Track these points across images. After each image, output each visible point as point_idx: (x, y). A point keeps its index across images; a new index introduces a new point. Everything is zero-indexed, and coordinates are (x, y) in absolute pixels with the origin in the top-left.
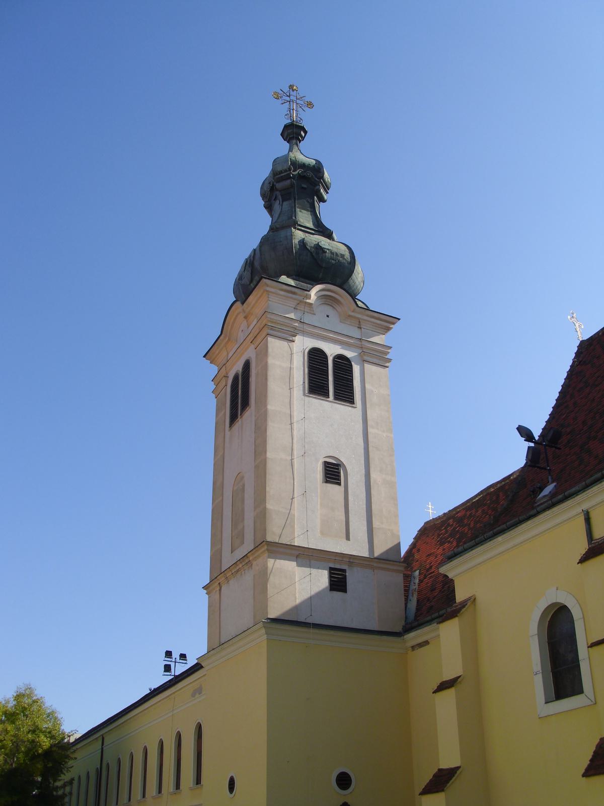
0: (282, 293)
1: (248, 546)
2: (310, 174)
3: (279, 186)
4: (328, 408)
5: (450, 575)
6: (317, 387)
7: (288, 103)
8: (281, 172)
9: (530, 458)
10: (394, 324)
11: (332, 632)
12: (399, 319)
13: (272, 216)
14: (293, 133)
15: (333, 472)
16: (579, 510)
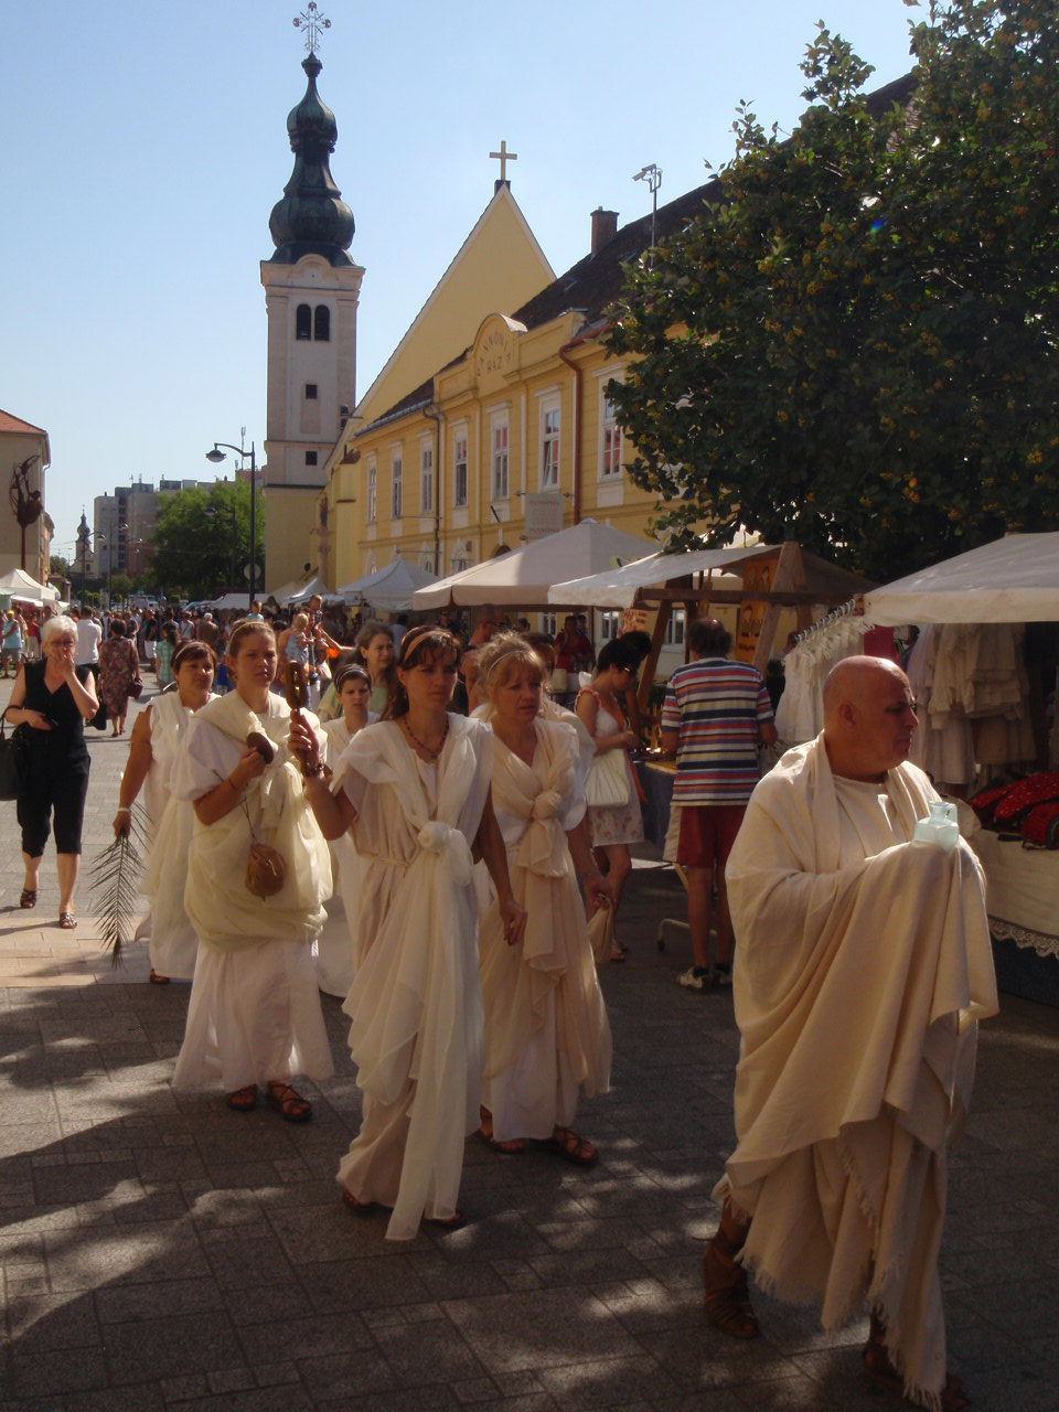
14: (312, 67)
15: (311, 391)
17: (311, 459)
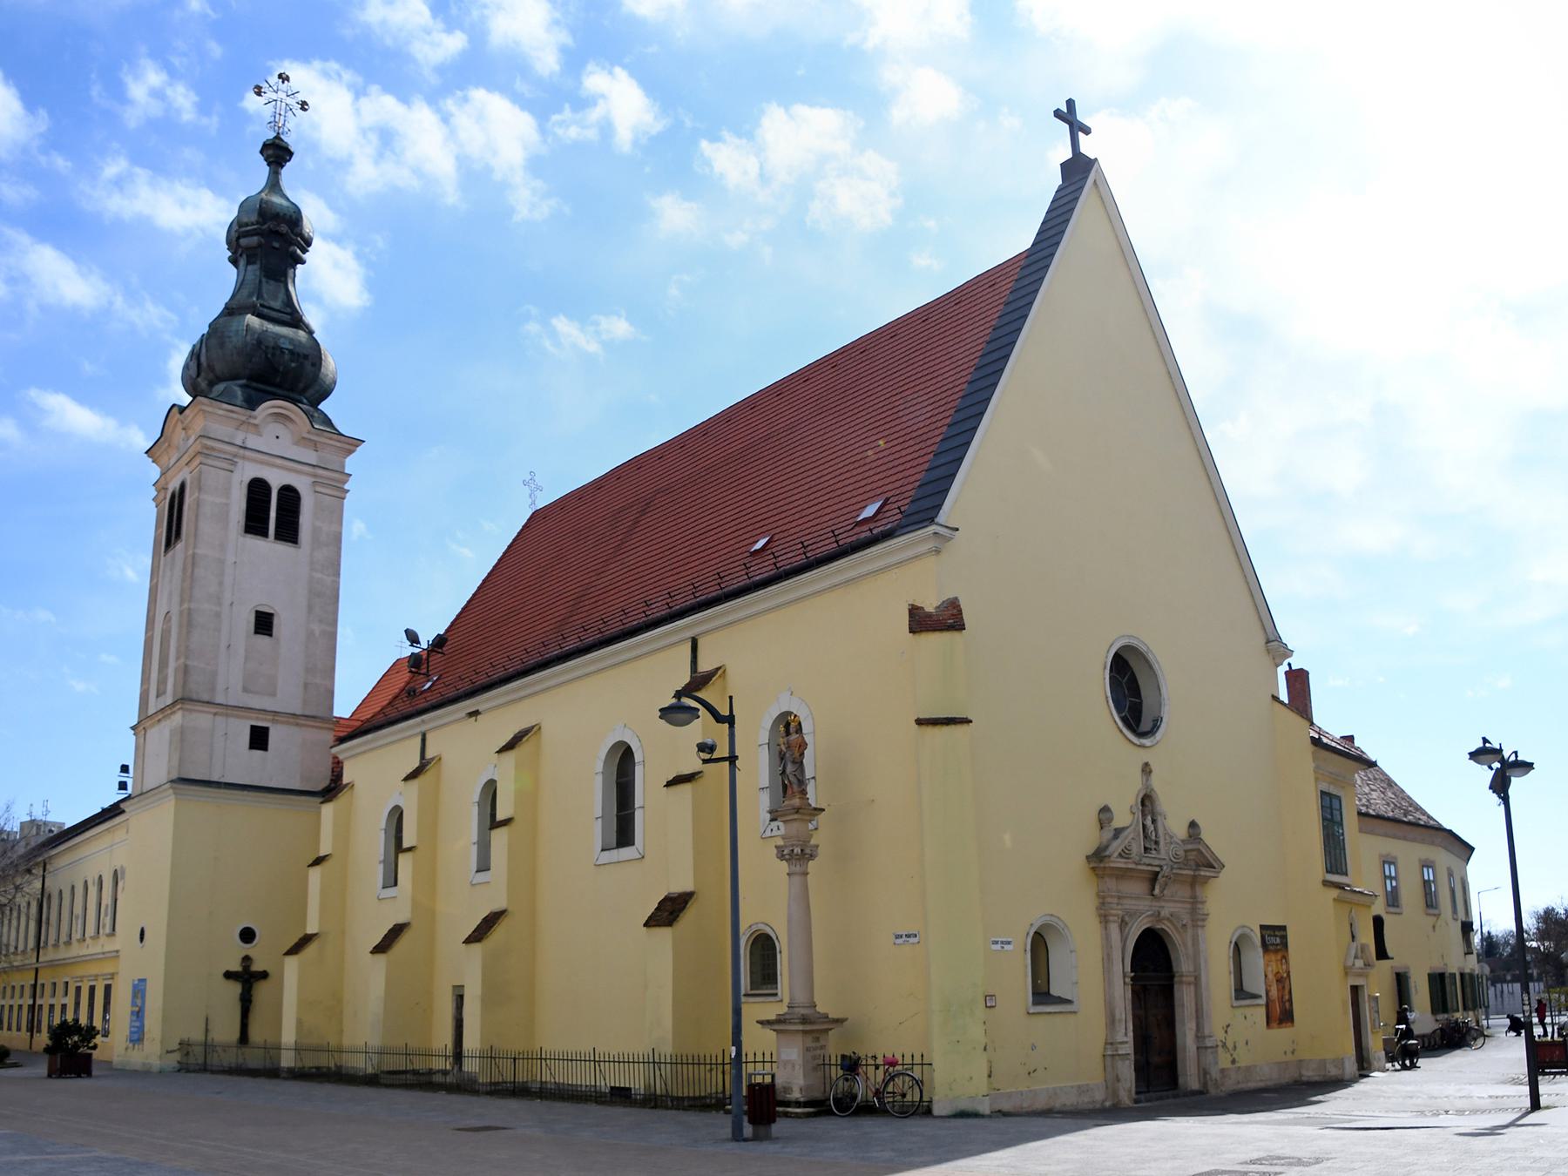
1: (168, 699)
2: (284, 228)
3: (243, 241)
4: (268, 548)
5: (341, 757)
6: (255, 523)
15: (264, 623)
16: (419, 730)
17: (259, 739)
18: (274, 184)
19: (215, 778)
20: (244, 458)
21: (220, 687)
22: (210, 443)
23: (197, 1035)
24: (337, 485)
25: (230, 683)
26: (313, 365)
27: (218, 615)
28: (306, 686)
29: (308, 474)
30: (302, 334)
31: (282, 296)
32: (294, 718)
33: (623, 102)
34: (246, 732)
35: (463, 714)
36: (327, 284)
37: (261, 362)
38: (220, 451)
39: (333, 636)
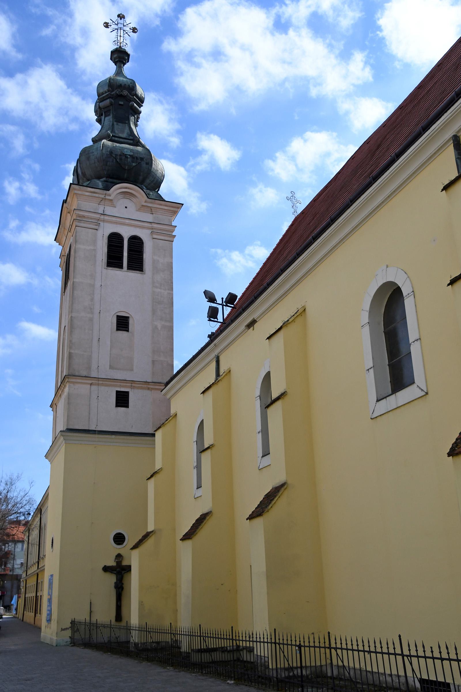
0: (87, 194)
2: (125, 93)
4: (123, 275)
6: (114, 260)
7: (116, 30)
8: (103, 94)
9: (210, 314)
10: (178, 208)
11: (128, 437)
12: (183, 204)
13: (100, 125)
15: (123, 323)
17: (122, 400)
18: (119, 72)
19: (93, 428)
20: (104, 221)
21: (94, 366)
22: (81, 213)
23: (82, 616)
24: (168, 234)
25: (101, 363)
26: (147, 164)
27: (91, 320)
28: (153, 362)
29: (148, 228)
30: (139, 149)
31: (127, 130)
32: (146, 385)
33: (220, 151)
34: (111, 400)
35: (243, 327)
36: (154, 123)
37: (118, 164)
38: (88, 218)
39: (171, 329)
